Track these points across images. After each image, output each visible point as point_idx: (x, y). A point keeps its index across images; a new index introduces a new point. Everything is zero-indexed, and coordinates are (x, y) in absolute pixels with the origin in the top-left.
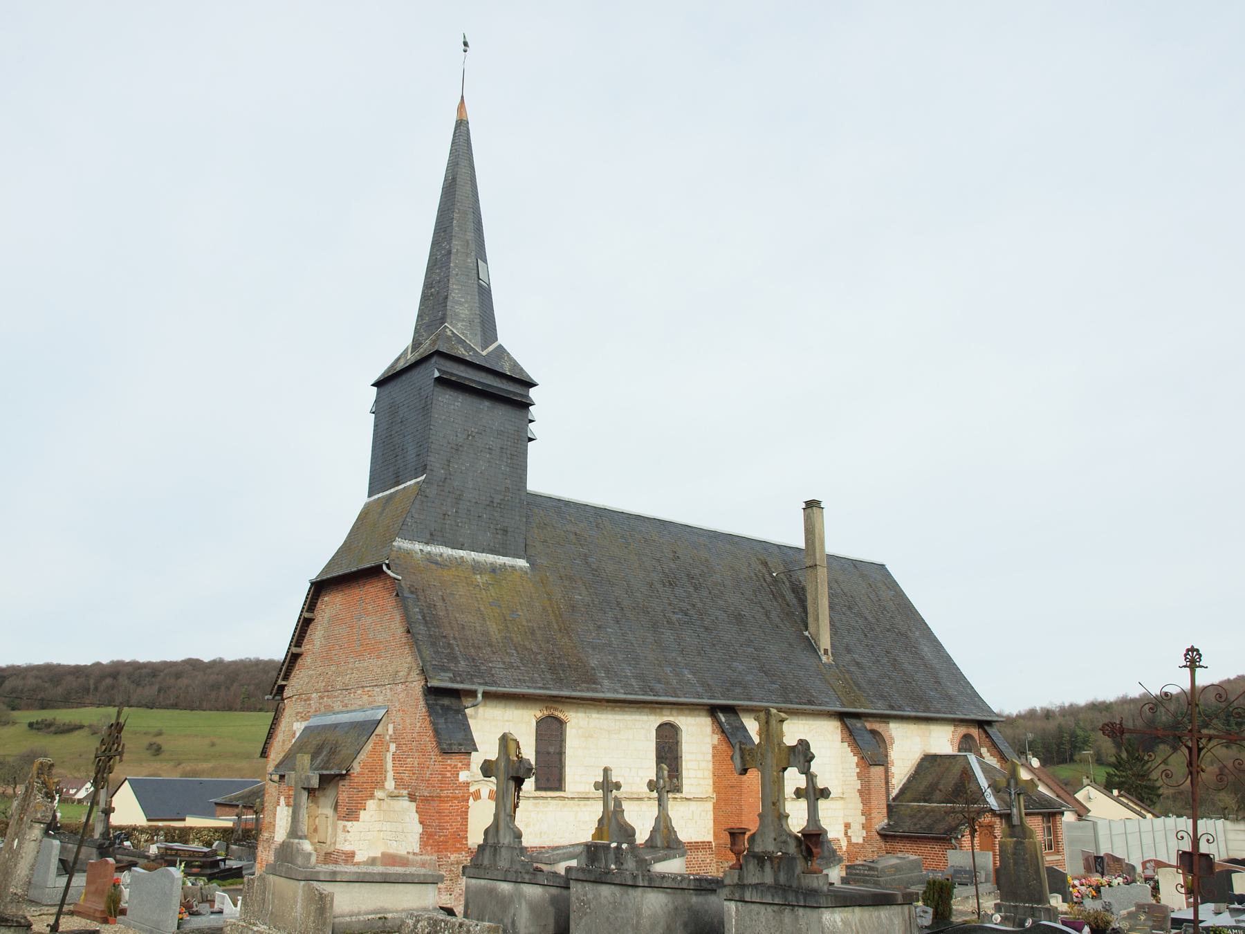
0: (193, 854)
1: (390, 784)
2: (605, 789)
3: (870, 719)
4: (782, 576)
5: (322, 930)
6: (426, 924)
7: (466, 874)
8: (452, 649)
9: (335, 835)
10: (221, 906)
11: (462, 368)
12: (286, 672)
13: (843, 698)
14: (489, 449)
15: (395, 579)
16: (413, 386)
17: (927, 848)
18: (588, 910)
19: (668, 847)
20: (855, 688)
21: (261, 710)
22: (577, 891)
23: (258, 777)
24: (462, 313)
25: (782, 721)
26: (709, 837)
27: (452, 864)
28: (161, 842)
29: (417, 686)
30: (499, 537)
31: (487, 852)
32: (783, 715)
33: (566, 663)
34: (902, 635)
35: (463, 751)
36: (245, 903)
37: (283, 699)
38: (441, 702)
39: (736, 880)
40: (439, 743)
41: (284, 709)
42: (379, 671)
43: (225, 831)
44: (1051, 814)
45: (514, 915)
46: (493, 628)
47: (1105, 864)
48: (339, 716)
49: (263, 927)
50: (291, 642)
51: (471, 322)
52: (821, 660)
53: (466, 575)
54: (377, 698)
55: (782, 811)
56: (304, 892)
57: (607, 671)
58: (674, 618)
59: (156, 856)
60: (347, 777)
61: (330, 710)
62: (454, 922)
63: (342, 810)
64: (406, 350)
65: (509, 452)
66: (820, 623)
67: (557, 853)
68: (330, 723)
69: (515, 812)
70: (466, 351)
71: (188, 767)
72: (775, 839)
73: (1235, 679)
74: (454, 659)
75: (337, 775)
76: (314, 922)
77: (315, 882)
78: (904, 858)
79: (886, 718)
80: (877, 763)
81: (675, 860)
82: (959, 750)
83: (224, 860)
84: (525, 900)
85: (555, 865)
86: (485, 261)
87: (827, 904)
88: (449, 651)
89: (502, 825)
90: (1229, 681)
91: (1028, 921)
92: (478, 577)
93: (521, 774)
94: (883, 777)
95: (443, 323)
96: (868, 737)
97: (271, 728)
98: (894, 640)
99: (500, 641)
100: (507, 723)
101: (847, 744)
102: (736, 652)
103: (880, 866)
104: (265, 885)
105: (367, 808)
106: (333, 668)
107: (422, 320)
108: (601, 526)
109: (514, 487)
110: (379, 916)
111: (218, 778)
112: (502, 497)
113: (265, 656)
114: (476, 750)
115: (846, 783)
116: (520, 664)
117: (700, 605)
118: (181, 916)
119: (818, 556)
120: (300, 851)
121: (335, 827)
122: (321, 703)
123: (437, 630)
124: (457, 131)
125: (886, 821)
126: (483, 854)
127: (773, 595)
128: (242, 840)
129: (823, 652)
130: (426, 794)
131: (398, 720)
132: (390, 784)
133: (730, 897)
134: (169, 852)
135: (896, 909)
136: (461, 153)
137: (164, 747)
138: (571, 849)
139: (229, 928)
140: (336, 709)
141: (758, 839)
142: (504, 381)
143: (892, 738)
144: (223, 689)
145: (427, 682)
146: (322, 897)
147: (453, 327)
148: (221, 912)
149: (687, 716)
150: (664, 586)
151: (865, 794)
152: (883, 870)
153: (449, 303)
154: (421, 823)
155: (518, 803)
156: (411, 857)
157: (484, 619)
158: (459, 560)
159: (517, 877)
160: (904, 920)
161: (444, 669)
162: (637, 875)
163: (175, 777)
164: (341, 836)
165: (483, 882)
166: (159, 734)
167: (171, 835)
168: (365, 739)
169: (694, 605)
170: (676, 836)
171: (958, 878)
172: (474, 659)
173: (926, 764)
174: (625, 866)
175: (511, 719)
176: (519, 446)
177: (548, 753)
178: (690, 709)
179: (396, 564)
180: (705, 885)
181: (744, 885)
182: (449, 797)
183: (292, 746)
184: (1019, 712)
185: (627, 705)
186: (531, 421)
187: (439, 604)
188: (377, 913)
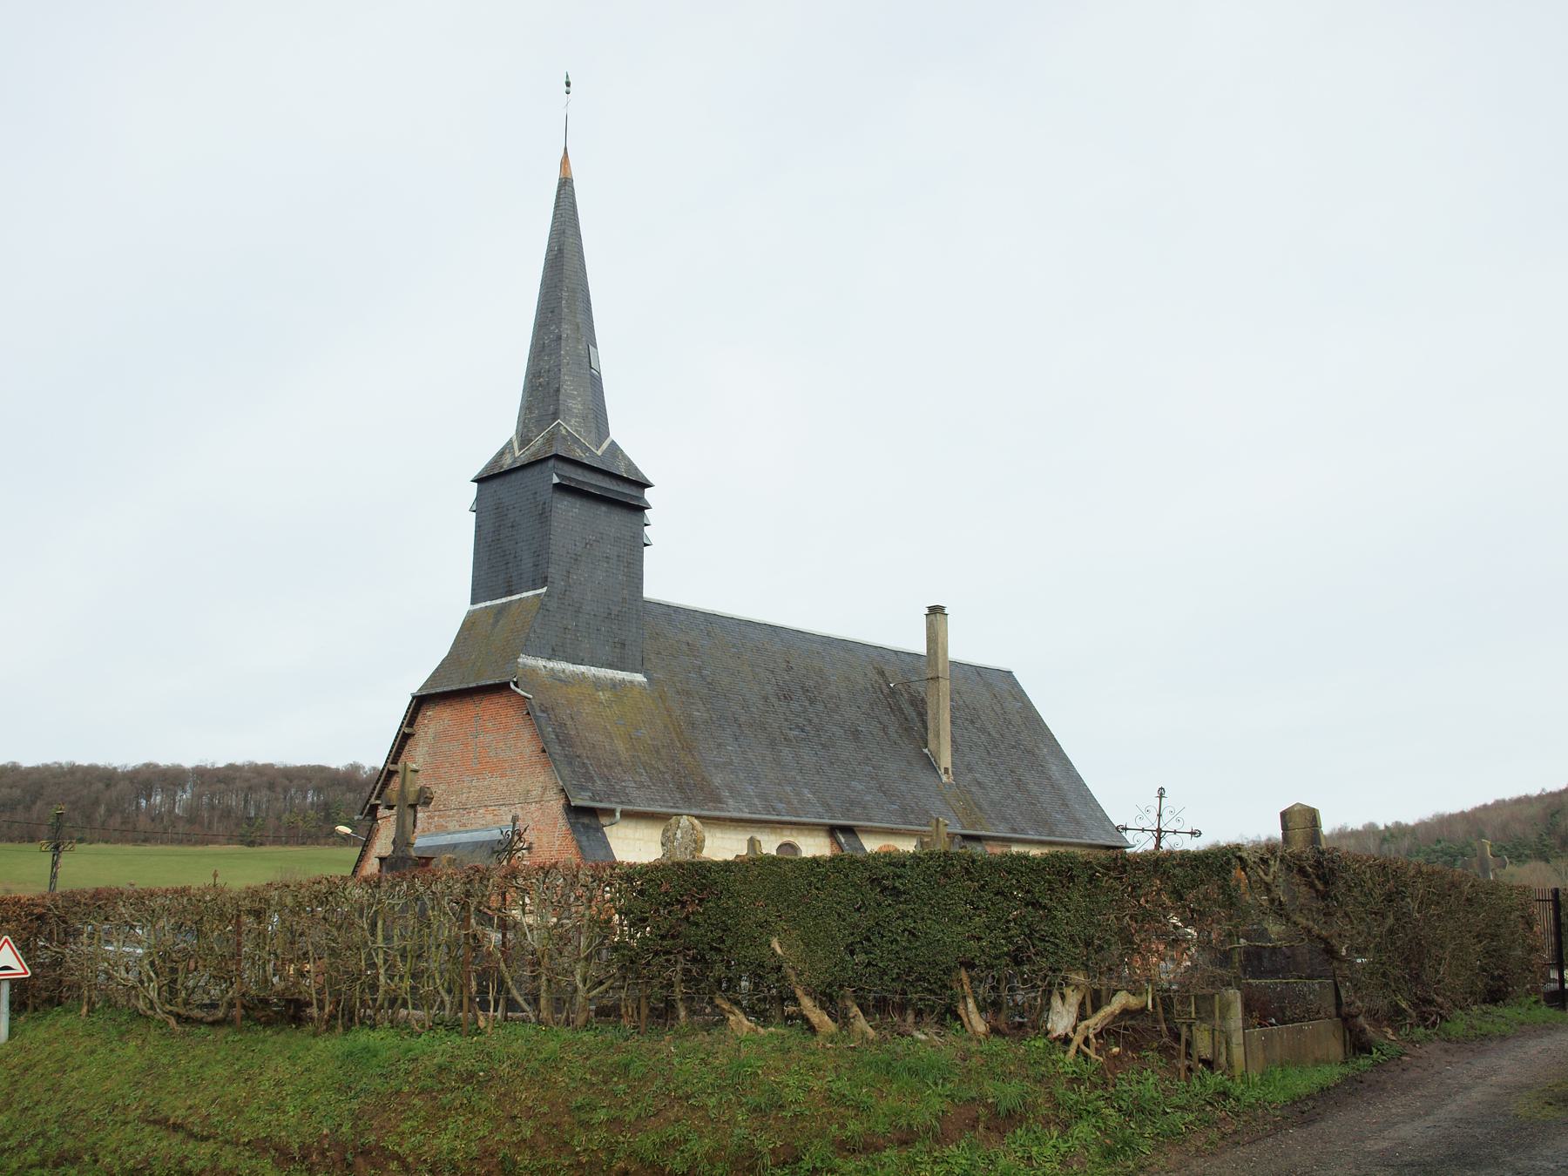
4: (900, 687)
8: (587, 769)
11: (580, 471)
13: (963, 820)
14: (607, 557)
16: (526, 489)
20: (976, 809)
29: (556, 805)
34: (1028, 752)
38: (581, 821)
42: (504, 790)
46: (621, 746)
48: (456, 836)
50: (388, 758)
51: (585, 418)
52: (941, 780)
57: (731, 791)
61: (442, 829)
64: (510, 442)
65: (625, 560)
68: (445, 843)
73: (1493, 805)
86: (595, 347)
90: (1485, 807)
92: (601, 693)
98: (1019, 758)
100: (638, 842)
102: (854, 771)
106: (443, 787)
109: (631, 597)
112: (620, 609)
116: (650, 784)
117: (816, 720)
123: (571, 749)
124: (562, 192)
127: (891, 708)
129: (943, 771)
147: (566, 424)
150: (779, 700)
153: (561, 397)
161: (583, 788)
169: (810, 721)
176: (635, 553)
178: (809, 829)
185: (748, 824)
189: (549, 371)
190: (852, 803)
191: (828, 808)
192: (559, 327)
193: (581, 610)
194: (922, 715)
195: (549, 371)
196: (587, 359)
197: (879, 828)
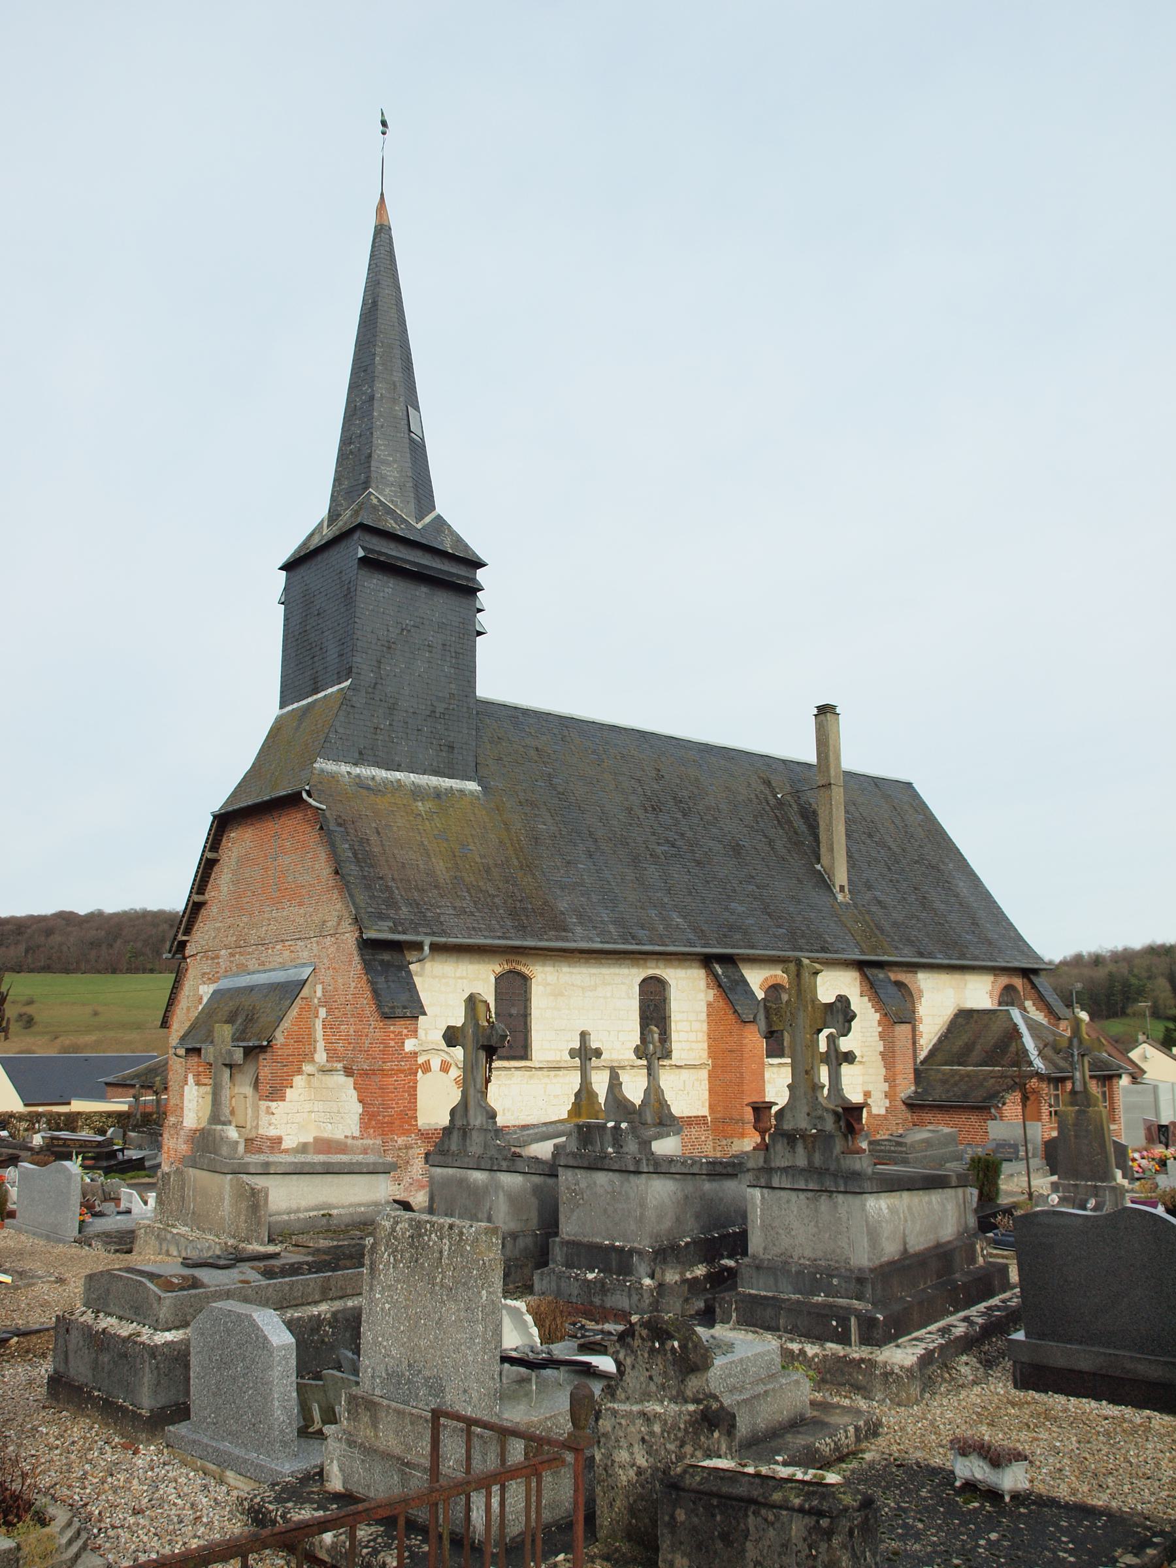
0: (84, 1144)
1: (321, 1056)
2: (583, 1056)
3: (895, 969)
4: (789, 798)
5: (256, 1231)
6: (407, 1226)
7: (430, 1163)
8: (392, 892)
9: (257, 1117)
10: (128, 1205)
11: (392, 545)
12: (187, 925)
14: (429, 646)
15: (318, 808)
16: (331, 570)
17: (962, 1119)
18: (581, 1202)
19: (661, 1124)
20: (877, 932)
21: (152, 971)
22: (567, 1179)
23: (153, 1050)
24: (390, 476)
25: (816, 973)
26: (704, 1111)
27: (400, 1149)
28: (44, 1130)
29: (350, 938)
30: (444, 754)
31: (455, 1136)
32: (818, 966)
33: (529, 906)
35: (408, 1014)
36: (160, 1201)
37: (185, 958)
39: (761, 1163)
40: (379, 1006)
41: (186, 970)
43: (120, 1115)
44: (1107, 1078)
45: (490, 1209)
46: (440, 866)
47: (1170, 1134)
48: (255, 976)
49: (184, 1228)
50: (192, 888)
51: (402, 487)
52: (836, 899)
53: (405, 802)
54: (300, 954)
55: (816, 1080)
56: (231, 1188)
57: (580, 916)
58: (659, 850)
59: (41, 1147)
60: (269, 1049)
61: (243, 970)
62: (443, 1224)
63: (265, 1088)
65: (452, 650)
66: (835, 855)
67: (544, 1132)
68: (244, 985)
69: (487, 1088)
70: (396, 523)
71: (66, 1040)
72: (808, 1114)
74: (391, 903)
75: (255, 1047)
76: (246, 1222)
77: (245, 1176)
78: (938, 1131)
79: (913, 967)
80: (904, 1020)
81: (669, 1138)
82: (1000, 1004)
83: (122, 1150)
84: (503, 1191)
85: (526, 1148)
86: (417, 409)
87: (872, 1188)
88: (387, 895)
89: (472, 1103)
91: (1090, 1202)
93: (493, 1043)
94: (910, 1036)
95: (366, 488)
96: (892, 990)
97: (172, 993)
99: (449, 882)
101: (867, 998)
102: (734, 891)
103: (908, 1140)
104: (183, 1180)
105: (294, 1085)
106: (245, 919)
107: (340, 484)
108: (568, 739)
110: (322, 1212)
111: (104, 1052)
112: (446, 706)
113: (154, 904)
114: (424, 1014)
115: (867, 1044)
117: (689, 834)
118: (82, 1218)
119: (832, 773)
120: (224, 1140)
121: (256, 1109)
122: (231, 962)
123: (371, 870)
125: (913, 1088)
126: (449, 1139)
127: (778, 821)
128: (141, 1126)
129: (838, 889)
130: (365, 1067)
131: (328, 980)
132: (321, 1056)
133: (755, 1183)
134: (56, 1142)
135: (950, 1192)
136: (382, 269)
137: (37, 1018)
138: (544, 1129)
139: (142, 1231)
140: (251, 968)
141: (788, 1115)
142: (446, 562)
143: (921, 991)
144: (104, 947)
145: (361, 933)
146: (254, 1193)
148: (129, 1212)
149: (676, 968)
150: (646, 811)
151: (888, 1057)
152: (912, 1145)
153: (373, 464)
154: (360, 1102)
155: (490, 1077)
156: (350, 1141)
157: (429, 856)
158: (395, 784)
159: (492, 1164)
160: (958, 1205)
161: (382, 917)
162: (640, 1159)
163: (52, 1053)
164: (264, 1119)
165: (450, 1171)
166: (30, 1002)
167: (56, 1123)
168: (288, 1002)
169: (682, 835)
170: (669, 1109)
171: (1002, 1153)
172: (418, 904)
173: (960, 1020)
174: (625, 1149)
175: (465, 974)
177: (511, 1015)
178: (679, 960)
179: (318, 790)
180: (719, 1169)
181: (771, 1169)
182: (393, 1070)
183: (200, 1013)
184: (1065, 957)
185: (603, 956)
186: (479, 610)
187: (374, 838)
188: (320, 1210)
189: (360, 436)
190: (731, 928)
191: (702, 934)
192: (371, 387)
193: (396, 707)
194: (813, 829)
195: (360, 436)
196: (406, 422)
197: (763, 955)
